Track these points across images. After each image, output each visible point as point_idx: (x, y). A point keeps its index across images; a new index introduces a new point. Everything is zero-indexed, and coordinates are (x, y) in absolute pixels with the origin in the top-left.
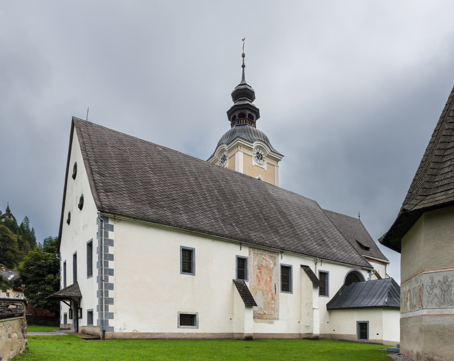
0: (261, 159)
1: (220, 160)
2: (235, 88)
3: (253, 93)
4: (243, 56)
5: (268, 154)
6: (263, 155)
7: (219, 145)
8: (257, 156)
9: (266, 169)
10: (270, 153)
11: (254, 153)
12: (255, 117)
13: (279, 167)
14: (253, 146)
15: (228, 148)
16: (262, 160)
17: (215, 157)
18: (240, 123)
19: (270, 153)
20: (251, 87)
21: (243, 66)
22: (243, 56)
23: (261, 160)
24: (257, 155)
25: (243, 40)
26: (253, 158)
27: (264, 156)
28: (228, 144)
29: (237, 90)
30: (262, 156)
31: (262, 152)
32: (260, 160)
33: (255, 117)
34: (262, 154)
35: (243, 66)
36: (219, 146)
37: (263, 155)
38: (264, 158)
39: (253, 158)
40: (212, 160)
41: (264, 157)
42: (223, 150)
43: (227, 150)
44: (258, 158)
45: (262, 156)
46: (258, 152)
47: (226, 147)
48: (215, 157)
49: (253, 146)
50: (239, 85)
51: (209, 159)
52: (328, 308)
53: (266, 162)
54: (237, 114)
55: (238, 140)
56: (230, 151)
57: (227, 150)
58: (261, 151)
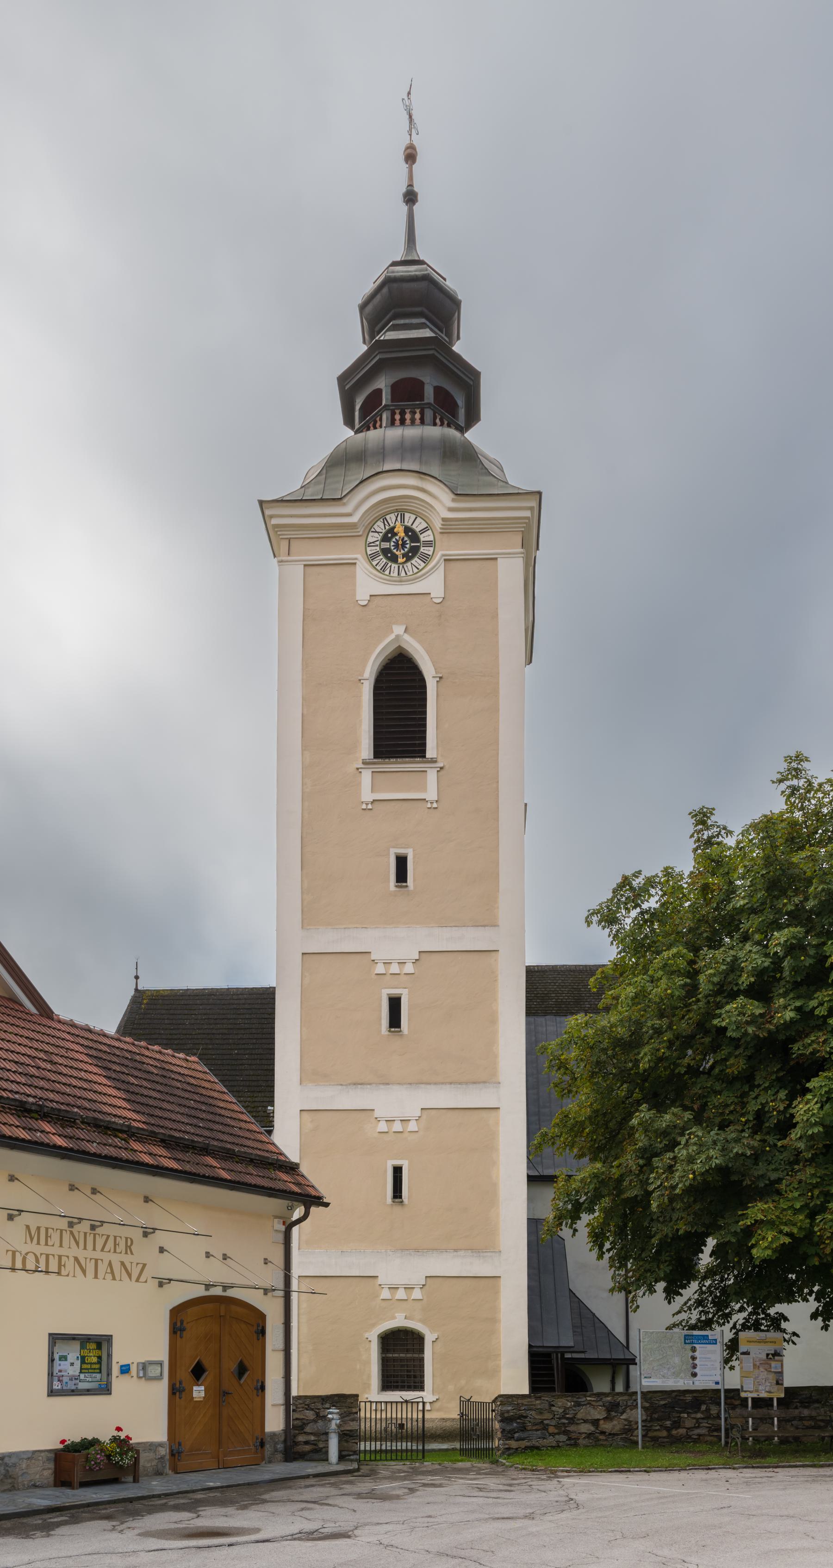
3: (457, 304)
4: (411, 157)
5: (444, 520)
8: (385, 552)
10: (451, 510)
11: (370, 539)
12: (462, 412)
16: (416, 561)
19: (451, 510)
21: (410, 197)
24: (386, 545)
26: (358, 568)
33: (462, 412)
34: (418, 530)
35: (410, 197)
38: (429, 544)
41: (431, 538)
49: (349, 515)
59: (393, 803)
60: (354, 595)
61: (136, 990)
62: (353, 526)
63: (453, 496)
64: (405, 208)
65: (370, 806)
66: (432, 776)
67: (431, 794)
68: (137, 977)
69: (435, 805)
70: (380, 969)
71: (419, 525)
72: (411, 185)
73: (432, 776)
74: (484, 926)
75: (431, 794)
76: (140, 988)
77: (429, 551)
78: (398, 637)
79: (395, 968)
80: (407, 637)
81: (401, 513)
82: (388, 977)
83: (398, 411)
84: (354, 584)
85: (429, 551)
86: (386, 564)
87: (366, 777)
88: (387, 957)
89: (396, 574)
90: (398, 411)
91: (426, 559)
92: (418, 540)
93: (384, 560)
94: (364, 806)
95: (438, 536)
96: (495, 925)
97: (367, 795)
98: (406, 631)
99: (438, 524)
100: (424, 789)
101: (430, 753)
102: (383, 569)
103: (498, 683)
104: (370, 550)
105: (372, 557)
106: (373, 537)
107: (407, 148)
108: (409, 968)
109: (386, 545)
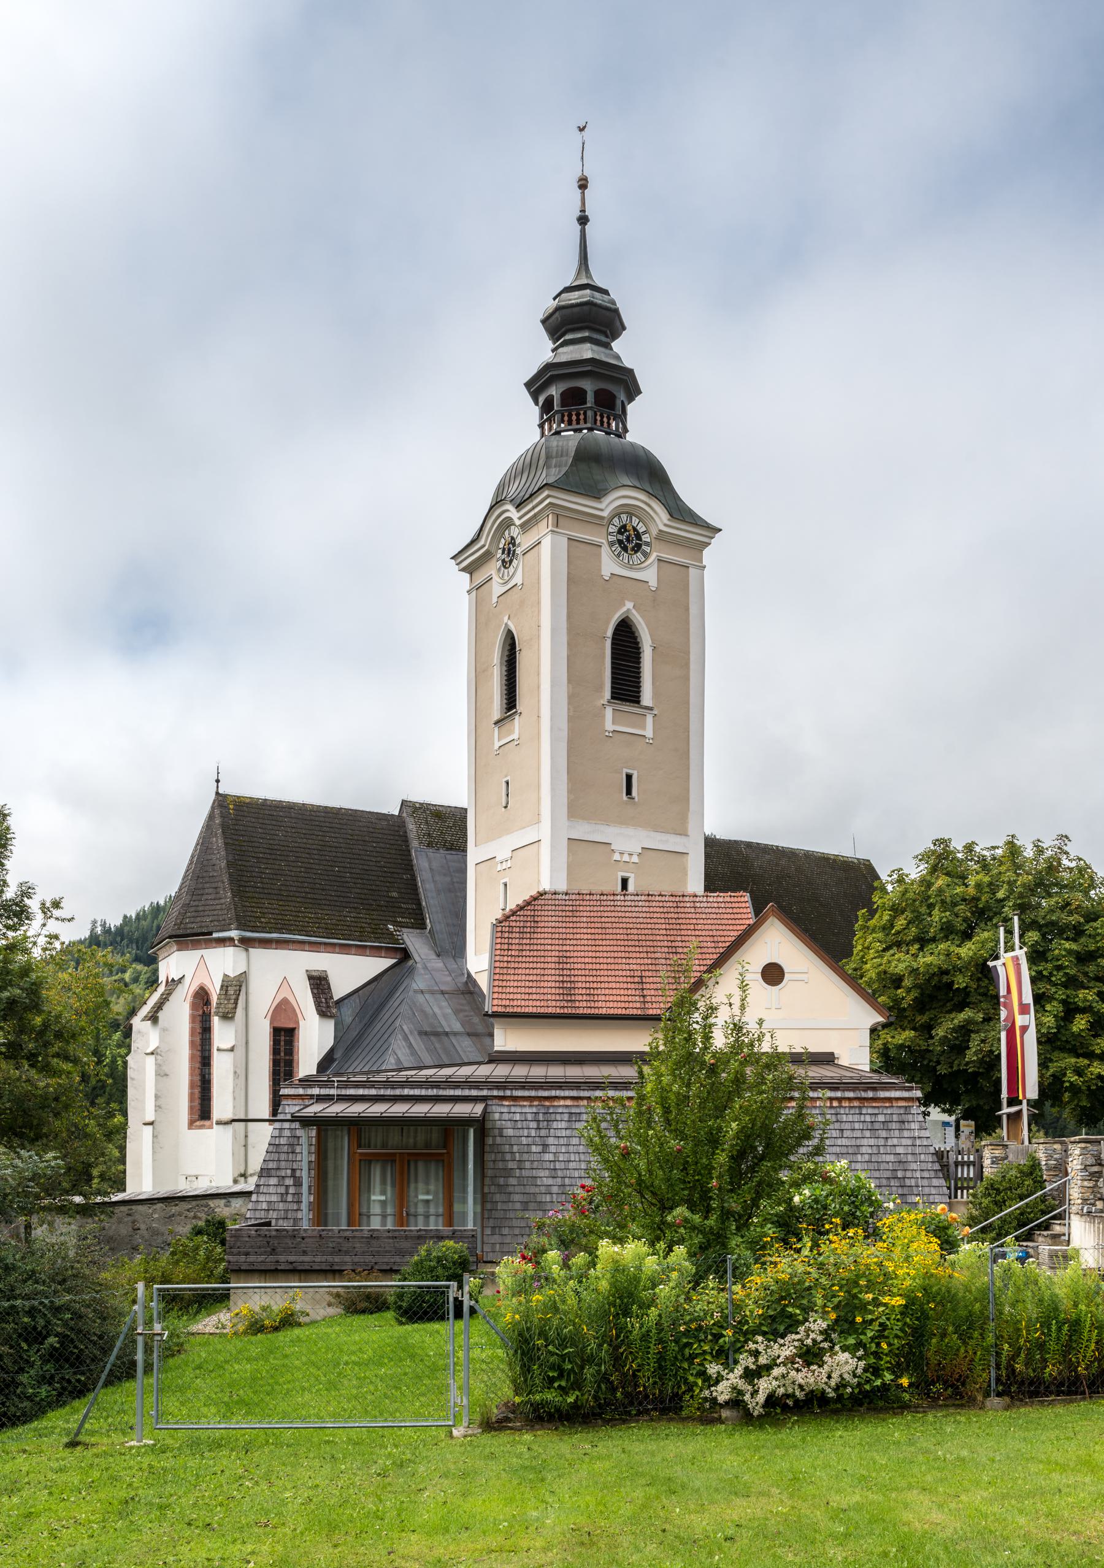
0: (637, 548)
1: (498, 556)
2: (554, 299)
3: (616, 312)
4: (583, 184)
5: (660, 531)
6: (645, 533)
7: (497, 503)
8: (620, 542)
9: (653, 583)
10: (665, 525)
11: (610, 530)
13: (705, 567)
14: (602, 510)
15: (520, 518)
16: (639, 554)
17: (484, 546)
18: (574, 422)
19: (665, 525)
20: (606, 292)
21: (583, 220)
22: (583, 184)
23: (636, 552)
24: (620, 537)
25: (582, 129)
27: (646, 538)
28: (518, 507)
29: (558, 309)
30: (638, 536)
31: (641, 524)
32: (629, 552)
34: (641, 531)
35: (583, 220)
36: (497, 503)
37: (645, 533)
38: (648, 544)
39: (605, 551)
40: (533, 508)
41: (649, 540)
42: (508, 523)
43: (518, 522)
44: (625, 549)
45: (641, 540)
46: (624, 527)
47: (513, 514)
48: (484, 546)
49: (602, 510)
50: (568, 290)
51: (460, 552)
52: (452, 856)
53: (653, 557)
54: (554, 391)
55: (548, 496)
56: (525, 527)
57: (518, 522)
58: (638, 521)
59: (626, 735)
60: (600, 570)
61: (217, 793)
62: (602, 518)
63: (669, 517)
64: (579, 227)
65: (611, 735)
66: (649, 719)
67: (649, 732)
68: (218, 781)
69: (651, 741)
70: (617, 857)
71: (641, 528)
72: (583, 211)
73: (649, 719)
74: (681, 835)
75: (649, 732)
76: (221, 792)
77: (647, 549)
78: (628, 610)
79: (626, 858)
80: (634, 611)
81: (630, 515)
82: (622, 863)
83: (598, 414)
84: (600, 562)
85: (647, 549)
86: (620, 552)
87: (609, 712)
88: (622, 849)
89: (626, 561)
90: (598, 414)
91: (646, 555)
92: (640, 539)
93: (619, 549)
94: (607, 734)
95: (653, 540)
96: (687, 835)
97: (609, 726)
98: (634, 607)
99: (654, 532)
100: (644, 728)
101: (647, 698)
102: (618, 556)
103: (689, 659)
104: (611, 538)
105: (611, 544)
106: (612, 529)
107: (580, 180)
108: (635, 859)
109: (620, 537)
